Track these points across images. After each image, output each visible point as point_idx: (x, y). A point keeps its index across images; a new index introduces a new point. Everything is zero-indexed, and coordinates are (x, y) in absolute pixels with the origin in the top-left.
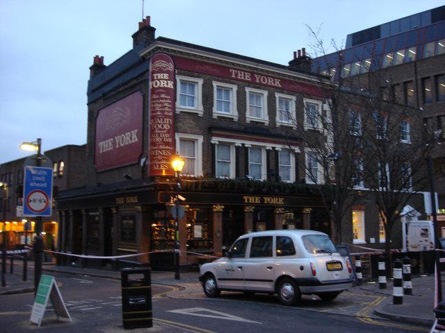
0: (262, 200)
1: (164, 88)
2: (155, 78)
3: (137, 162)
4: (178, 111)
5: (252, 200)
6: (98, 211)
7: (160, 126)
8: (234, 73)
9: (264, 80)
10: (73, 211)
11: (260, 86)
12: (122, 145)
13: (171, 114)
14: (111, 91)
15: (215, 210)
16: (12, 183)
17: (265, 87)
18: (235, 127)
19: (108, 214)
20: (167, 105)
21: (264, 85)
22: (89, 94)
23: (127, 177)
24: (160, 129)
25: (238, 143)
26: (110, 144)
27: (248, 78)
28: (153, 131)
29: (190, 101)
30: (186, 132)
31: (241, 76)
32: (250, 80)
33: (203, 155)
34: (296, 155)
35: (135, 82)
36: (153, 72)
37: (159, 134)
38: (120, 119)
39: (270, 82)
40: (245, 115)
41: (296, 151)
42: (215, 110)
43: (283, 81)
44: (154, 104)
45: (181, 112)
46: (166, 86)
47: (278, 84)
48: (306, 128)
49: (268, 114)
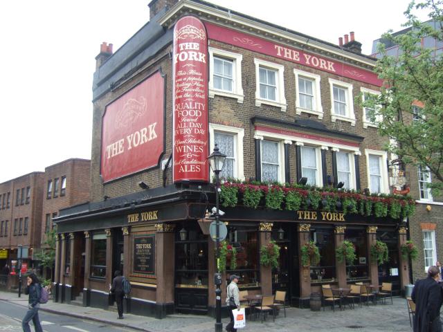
2: (182, 49)
3: (156, 165)
4: (212, 94)
6: (105, 233)
8: (279, 51)
9: (315, 63)
11: (310, 68)
12: (135, 145)
13: (203, 97)
14: (121, 80)
15: (262, 229)
16: (9, 205)
18: (283, 118)
19: (117, 233)
20: (198, 84)
21: (315, 68)
23: (143, 185)
24: (188, 117)
25: (288, 139)
26: (121, 146)
27: (296, 57)
28: (178, 119)
29: (228, 81)
31: (288, 55)
32: (298, 60)
33: (245, 154)
34: (357, 157)
35: (153, 61)
36: (179, 42)
37: (187, 122)
38: (132, 112)
39: (322, 64)
41: (357, 153)
42: (258, 94)
43: (337, 65)
44: (180, 83)
45: (216, 96)
46: (196, 59)
47: (331, 67)
48: (365, 126)
49: (322, 104)
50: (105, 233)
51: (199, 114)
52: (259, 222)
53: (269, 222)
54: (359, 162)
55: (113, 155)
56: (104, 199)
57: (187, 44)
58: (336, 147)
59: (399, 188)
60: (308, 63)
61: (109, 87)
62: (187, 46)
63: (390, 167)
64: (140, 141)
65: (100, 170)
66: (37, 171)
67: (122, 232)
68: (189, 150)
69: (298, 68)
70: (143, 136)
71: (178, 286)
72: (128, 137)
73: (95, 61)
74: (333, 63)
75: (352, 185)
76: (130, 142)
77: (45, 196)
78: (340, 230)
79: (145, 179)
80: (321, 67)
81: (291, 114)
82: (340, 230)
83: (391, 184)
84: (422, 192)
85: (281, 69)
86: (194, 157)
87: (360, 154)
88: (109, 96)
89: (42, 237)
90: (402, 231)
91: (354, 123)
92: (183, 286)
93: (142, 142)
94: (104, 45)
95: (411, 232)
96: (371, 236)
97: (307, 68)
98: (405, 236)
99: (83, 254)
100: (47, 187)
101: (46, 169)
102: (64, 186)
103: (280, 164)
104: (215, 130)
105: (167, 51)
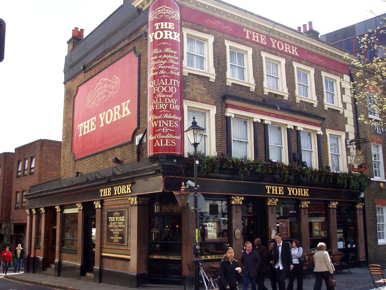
0: (286, 191)
1: (168, 40)
2: (157, 28)
4: (186, 72)
5: (275, 190)
6: (77, 207)
7: (164, 89)
10: (46, 208)
12: (108, 123)
14: (94, 61)
15: (233, 203)
17: (282, 54)
18: (252, 98)
19: (88, 208)
22: (65, 72)
23: (117, 161)
26: (92, 124)
30: (195, 100)
31: (256, 39)
32: (265, 43)
33: (217, 130)
34: (318, 136)
35: (127, 42)
38: (105, 91)
40: (262, 84)
41: (319, 133)
43: (299, 50)
45: (189, 74)
47: (294, 52)
50: (77, 207)
51: (174, 90)
52: (231, 196)
53: (240, 196)
54: (321, 141)
55: (85, 133)
56: (75, 175)
57: (162, 23)
58: (300, 127)
59: (356, 166)
60: (274, 46)
61: (82, 68)
62: (162, 25)
63: (348, 147)
64: (113, 118)
65: (72, 147)
66: (7, 151)
67: (94, 205)
68: (164, 124)
69: (265, 51)
70: (115, 113)
71: (151, 257)
72: (100, 115)
73: (67, 45)
74: (296, 48)
75: (315, 166)
76: (102, 119)
77: (15, 175)
78: (305, 204)
79: (118, 154)
80: (286, 51)
81: (259, 94)
82: (305, 204)
83: (349, 163)
84: (376, 171)
85: (250, 51)
86: (170, 132)
87: (322, 134)
88: (82, 77)
89: (12, 213)
90: (359, 206)
91: (316, 104)
92: (155, 257)
93: (115, 119)
94: (75, 30)
95: (366, 208)
96: (331, 210)
97: (273, 51)
98: (361, 211)
99: (54, 227)
100: (17, 166)
101: (16, 149)
102: (33, 166)
103: (249, 141)
104: (188, 107)
105: (141, 32)
